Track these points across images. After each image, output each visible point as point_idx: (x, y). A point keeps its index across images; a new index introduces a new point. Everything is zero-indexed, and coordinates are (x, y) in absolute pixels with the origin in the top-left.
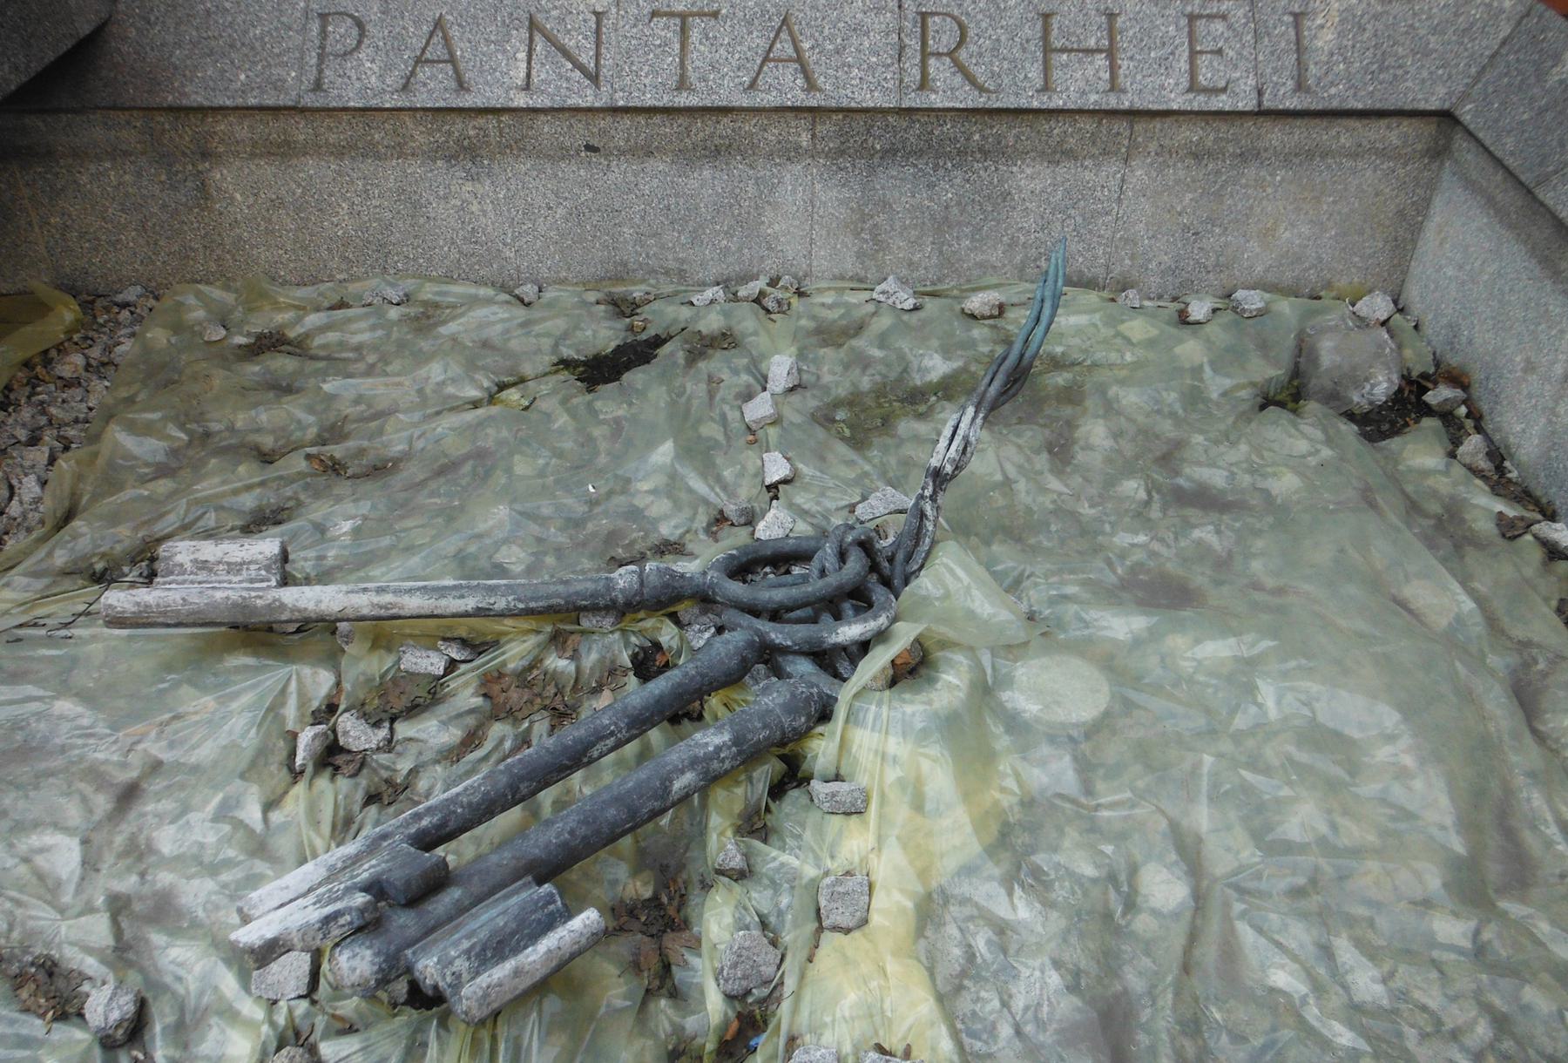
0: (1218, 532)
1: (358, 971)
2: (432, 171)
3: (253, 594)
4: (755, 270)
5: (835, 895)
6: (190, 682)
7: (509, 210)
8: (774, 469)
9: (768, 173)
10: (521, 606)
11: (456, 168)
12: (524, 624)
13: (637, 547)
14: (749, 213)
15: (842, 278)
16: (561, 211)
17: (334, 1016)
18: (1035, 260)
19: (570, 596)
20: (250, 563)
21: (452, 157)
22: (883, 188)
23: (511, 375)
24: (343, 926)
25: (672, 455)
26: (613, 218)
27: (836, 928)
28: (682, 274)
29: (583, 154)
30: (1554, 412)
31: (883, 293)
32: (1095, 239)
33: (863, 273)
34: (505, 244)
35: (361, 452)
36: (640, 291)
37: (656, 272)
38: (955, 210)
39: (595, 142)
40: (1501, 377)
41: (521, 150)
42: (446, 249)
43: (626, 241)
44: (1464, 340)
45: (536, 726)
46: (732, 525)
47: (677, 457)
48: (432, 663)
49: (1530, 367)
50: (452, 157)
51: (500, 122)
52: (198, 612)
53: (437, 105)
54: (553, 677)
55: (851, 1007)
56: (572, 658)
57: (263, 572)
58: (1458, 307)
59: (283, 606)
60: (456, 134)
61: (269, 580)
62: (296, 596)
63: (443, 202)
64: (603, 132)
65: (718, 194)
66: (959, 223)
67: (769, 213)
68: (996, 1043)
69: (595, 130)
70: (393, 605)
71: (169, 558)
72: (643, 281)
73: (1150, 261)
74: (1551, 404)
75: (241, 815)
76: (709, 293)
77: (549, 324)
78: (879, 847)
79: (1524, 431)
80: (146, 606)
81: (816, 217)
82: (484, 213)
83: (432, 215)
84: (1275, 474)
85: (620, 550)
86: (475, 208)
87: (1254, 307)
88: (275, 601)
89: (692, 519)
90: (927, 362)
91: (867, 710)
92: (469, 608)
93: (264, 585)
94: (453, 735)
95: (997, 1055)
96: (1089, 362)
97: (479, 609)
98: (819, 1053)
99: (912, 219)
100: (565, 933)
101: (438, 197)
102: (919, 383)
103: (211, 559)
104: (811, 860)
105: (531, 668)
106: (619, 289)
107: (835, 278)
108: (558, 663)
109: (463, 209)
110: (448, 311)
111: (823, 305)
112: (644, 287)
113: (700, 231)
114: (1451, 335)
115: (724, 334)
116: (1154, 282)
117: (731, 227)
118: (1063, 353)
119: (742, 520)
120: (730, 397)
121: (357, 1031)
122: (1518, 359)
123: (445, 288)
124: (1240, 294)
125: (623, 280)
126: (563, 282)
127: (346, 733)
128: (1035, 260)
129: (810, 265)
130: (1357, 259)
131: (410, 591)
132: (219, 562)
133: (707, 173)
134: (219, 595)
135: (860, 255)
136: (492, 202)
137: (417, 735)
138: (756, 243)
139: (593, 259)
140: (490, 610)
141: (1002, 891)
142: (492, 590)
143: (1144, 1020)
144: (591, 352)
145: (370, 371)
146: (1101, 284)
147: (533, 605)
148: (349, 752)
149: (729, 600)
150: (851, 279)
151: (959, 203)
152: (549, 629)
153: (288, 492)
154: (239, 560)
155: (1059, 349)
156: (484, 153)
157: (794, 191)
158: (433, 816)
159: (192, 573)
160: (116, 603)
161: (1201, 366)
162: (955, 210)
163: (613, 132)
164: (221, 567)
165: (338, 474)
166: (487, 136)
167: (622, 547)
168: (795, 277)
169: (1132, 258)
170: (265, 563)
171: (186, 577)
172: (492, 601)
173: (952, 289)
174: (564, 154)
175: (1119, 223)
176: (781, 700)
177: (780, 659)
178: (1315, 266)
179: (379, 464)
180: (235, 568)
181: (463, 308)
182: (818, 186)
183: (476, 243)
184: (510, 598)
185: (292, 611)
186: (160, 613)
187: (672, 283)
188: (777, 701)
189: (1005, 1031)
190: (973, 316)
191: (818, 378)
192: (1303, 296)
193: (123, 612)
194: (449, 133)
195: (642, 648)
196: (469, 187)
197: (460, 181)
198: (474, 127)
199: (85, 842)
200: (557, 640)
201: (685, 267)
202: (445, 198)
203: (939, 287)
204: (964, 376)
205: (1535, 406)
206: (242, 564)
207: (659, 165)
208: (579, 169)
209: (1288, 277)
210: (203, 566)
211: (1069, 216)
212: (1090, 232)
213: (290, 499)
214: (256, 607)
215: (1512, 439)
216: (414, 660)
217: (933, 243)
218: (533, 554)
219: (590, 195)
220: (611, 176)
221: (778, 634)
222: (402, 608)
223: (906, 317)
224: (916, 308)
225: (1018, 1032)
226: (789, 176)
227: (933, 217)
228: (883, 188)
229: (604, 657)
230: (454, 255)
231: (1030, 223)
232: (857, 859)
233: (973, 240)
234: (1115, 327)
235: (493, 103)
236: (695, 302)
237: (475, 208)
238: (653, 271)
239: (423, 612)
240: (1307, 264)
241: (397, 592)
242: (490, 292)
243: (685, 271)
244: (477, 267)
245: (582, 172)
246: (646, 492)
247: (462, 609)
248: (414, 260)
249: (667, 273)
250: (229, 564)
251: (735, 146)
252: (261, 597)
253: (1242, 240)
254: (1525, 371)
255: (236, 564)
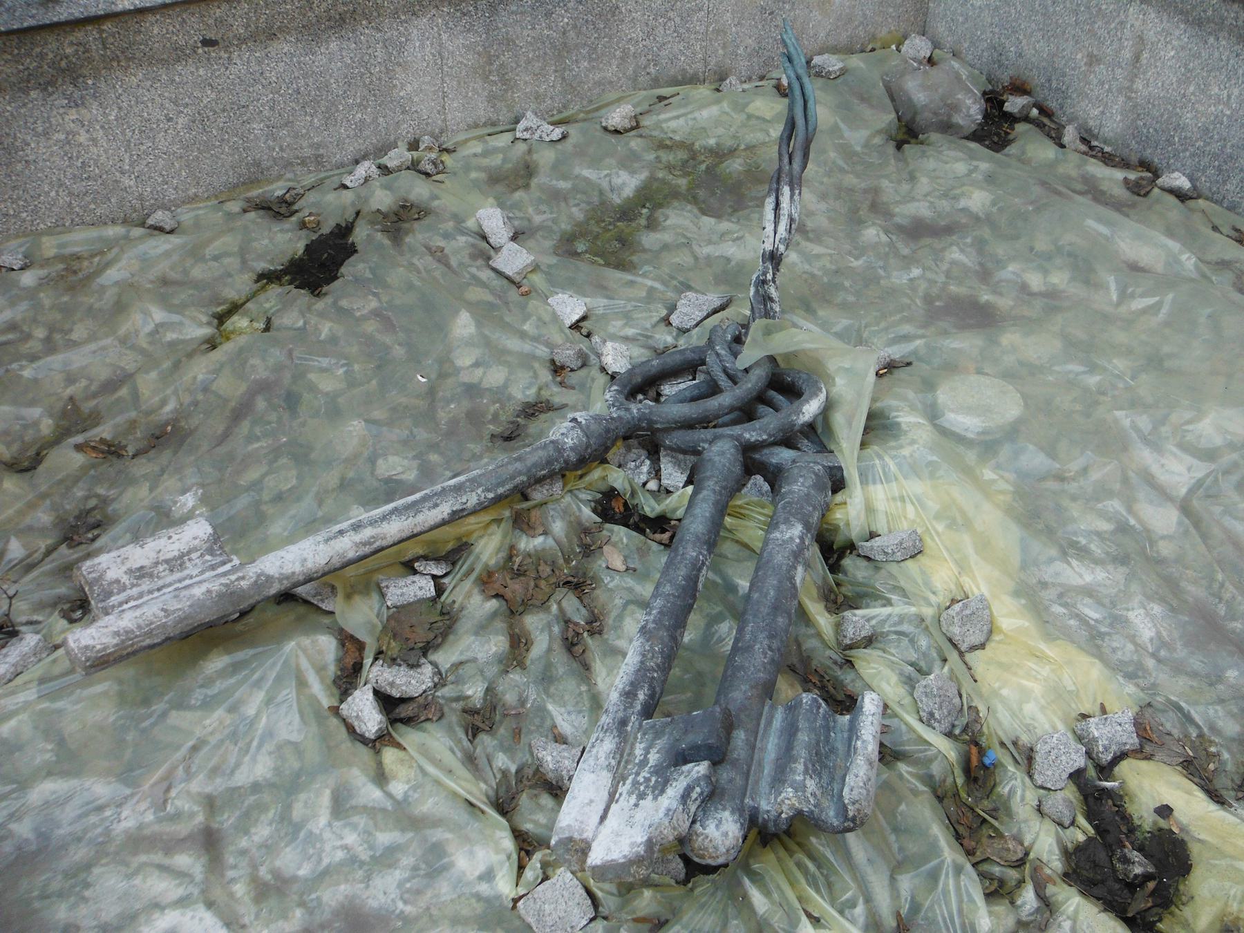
0: (962, 251)
1: (730, 834)
2: (25, 105)
3: (233, 577)
4: (392, 138)
5: (965, 619)
6: (180, 705)
7: (123, 133)
8: (568, 310)
9: (396, 33)
10: (491, 495)
11: (55, 96)
12: (485, 517)
13: (503, 418)
14: (380, 79)
15: (476, 126)
16: (182, 121)
17: (636, 920)
18: (645, 68)
19: (529, 470)
20: (189, 552)
21: (49, 83)
22: (505, 26)
23: (220, 304)
24: (696, 799)
25: (473, 323)
26: (241, 115)
27: (973, 648)
28: (318, 160)
29: (200, 51)
30: (1130, 89)
31: (526, 130)
32: (692, 37)
33: (494, 117)
34: (123, 173)
35: (133, 424)
36: (281, 188)
37: (291, 164)
38: (572, 34)
39: (211, 35)
40: (1064, 75)
41: (128, 59)
42: (53, 194)
43: (257, 138)
44: (1012, 55)
45: (564, 604)
46: (572, 370)
47: (479, 324)
48: (419, 587)
49: (1093, 60)
50: (49, 83)
51: (101, 32)
52: (185, 618)
53: (25, 25)
54: (538, 557)
55: (1043, 697)
56: (545, 533)
57: (208, 557)
58: (997, 30)
59: (269, 579)
60: (51, 56)
61: (231, 561)
62: (278, 564)
63: (43, 139)
64: (220, 22)
65: (347, 66)
66: (576, 45)
67: (400, 74)
68: (1150, 675)
69: (211, 21)
70: (374, 538)
71: (101, 577)
72: (279, 177)
73: (738, 47)
74: (1127, 84)
75: (360, 800)
76: (362, 170)
77: (217, 243)
78: (962, 566)
79: (1103, 113)
80: (127, 632)
81: (445, 68)
82: (94, 141)
83: (31, 158)
84: (963, 194)
85: (491, 427)
86: (83, 138)
87: (836, 68)
88: (259, 576)
89: (536, 376)
90: (617, 181)
91: (873, 466)
92: (445, 515)
93: (228, 567)
94: (497, 644)
95: (1158, 682)
96: (743, 147)
97: (454, 513)
98: (1054, 739)
99: (534, 51)
100: (870, 718)
101: (37, 135)
102: (619, 201)
103: (146, 563)
104: (922, 602)
105: (510, 557)
106: (255, 193)
107: (470, 127)
108: (529, 543)
109: (69, 143)
110: (96, 260)
111: (475, 155)
112: (280, 184)
113: (333, 109)
114: (995, 55)
115: (403, 207)
116: (743, 65)
117: (364, 98)
118: (717, 144)
119: (579, 364)
120: (467, 260)
121: (667, 921)
122: (1079, 56)
123: (66, 238)
124: (817, 60)
125: (259, 181)
126: (194, 199)
127: (392, 684)
128: (645, 68)
129: (445, 120)
130: (891, 10)
131: (384, 518)
132: (157, 563)
133: (333, 46)
134: (198, 592)
135: (491, 98)
136: (102, 127)
137: (463, 658)
138: (391, 110)
139: (223, 165)
140: (463, 510)
141: (1065, 566)
142: (458, 489)
143: (1222, 613)
144: (286, 259)
145: (50, 347)
146: (702, 78)
147: (501, 490)
148: (411, 699)
149: (676, 422)
150: (485, 125)
151: (575, 27)
152: (507, 513)
153: (79, 493)
154: (176, 553)
155: (712, 142)
156: (85, 72)
157: (422, 46)
158: (642, 687)
159: (133, 586)
160: (91, 642)
161: (836, 124)
162: (572, 34)
163: (230, 20)
164: (161, 568)
165: (120, 456)
166: (86, 51)
167: (490, 422)
168: (432, 135)
169: (724, 47)
170: (205, 547)
171: (129, 592)
172: (464, 501)
173: (577, 114)
174: (179, 55)
175: (711, 16)
176: (809, 482)
177: (757, 456)
178: (862, 23)
179: (158, 433)
180: (176, 563)
181: (115, 251)
182: (445, 37)
183: (88, 178)
184: (479, 491)
185: (280, 580)
186: (146, 633)
187: (310, 172)
188: (807, 485)
189: (1150, 663)
190: (617, 132)
191: (529, 220)
192: (856, 52)
193: (104, 649)
194: (42, 56)
195: (596, 502)
196: (73, 114)
197: (62, 111)
198: (72, 44)
199: (210, 905)
200: (521, 522)
201: (321, 151)
202: (46, 134)
203: (565, 114)
204: (655, 185)
205: (1110, 90)
206: (182, 556)
207: (283, 47)
208: (197, 69)
209: (843, 38)
210: (141, 573)
211: (670, 19)
212: (688, 30)
213: (87, 498)
214: (242, 590)
215: (1091, 123)
216: (399, 592)
217: (556, 71)
218: (415, 457)
219: (213, 96)
220: (233, 69)
221: (751, 433)
222: (384, 538)
223: (559, 146)
224: (564, 137)
225: (1159, 661)
226: (415, 32)
227: (554, 46)
228: (505, 26)
229: (571, 522)
230: (64, 199)
231: (637, 33)
232: (953, 587)
233: (591, 60)
234: (743, 110)
235: (93, 11)
236: (349, 184)
237: (83, 138)
238: (288, 164)
239: (404, 535)
240: (856, 23)
241: (373, 523)
242: (118, 230)
243: (322, 156)
244: (93, 206)
245: (201, 72)
246: (472, 366)
247: (440, 517)
248: (15, 216)
249: (303, 163)
250: (167, 561)
251: (359, 11)
252: (243, 578)
253: (807, 11)
254: (1090, 64)
255: (175, 559)
